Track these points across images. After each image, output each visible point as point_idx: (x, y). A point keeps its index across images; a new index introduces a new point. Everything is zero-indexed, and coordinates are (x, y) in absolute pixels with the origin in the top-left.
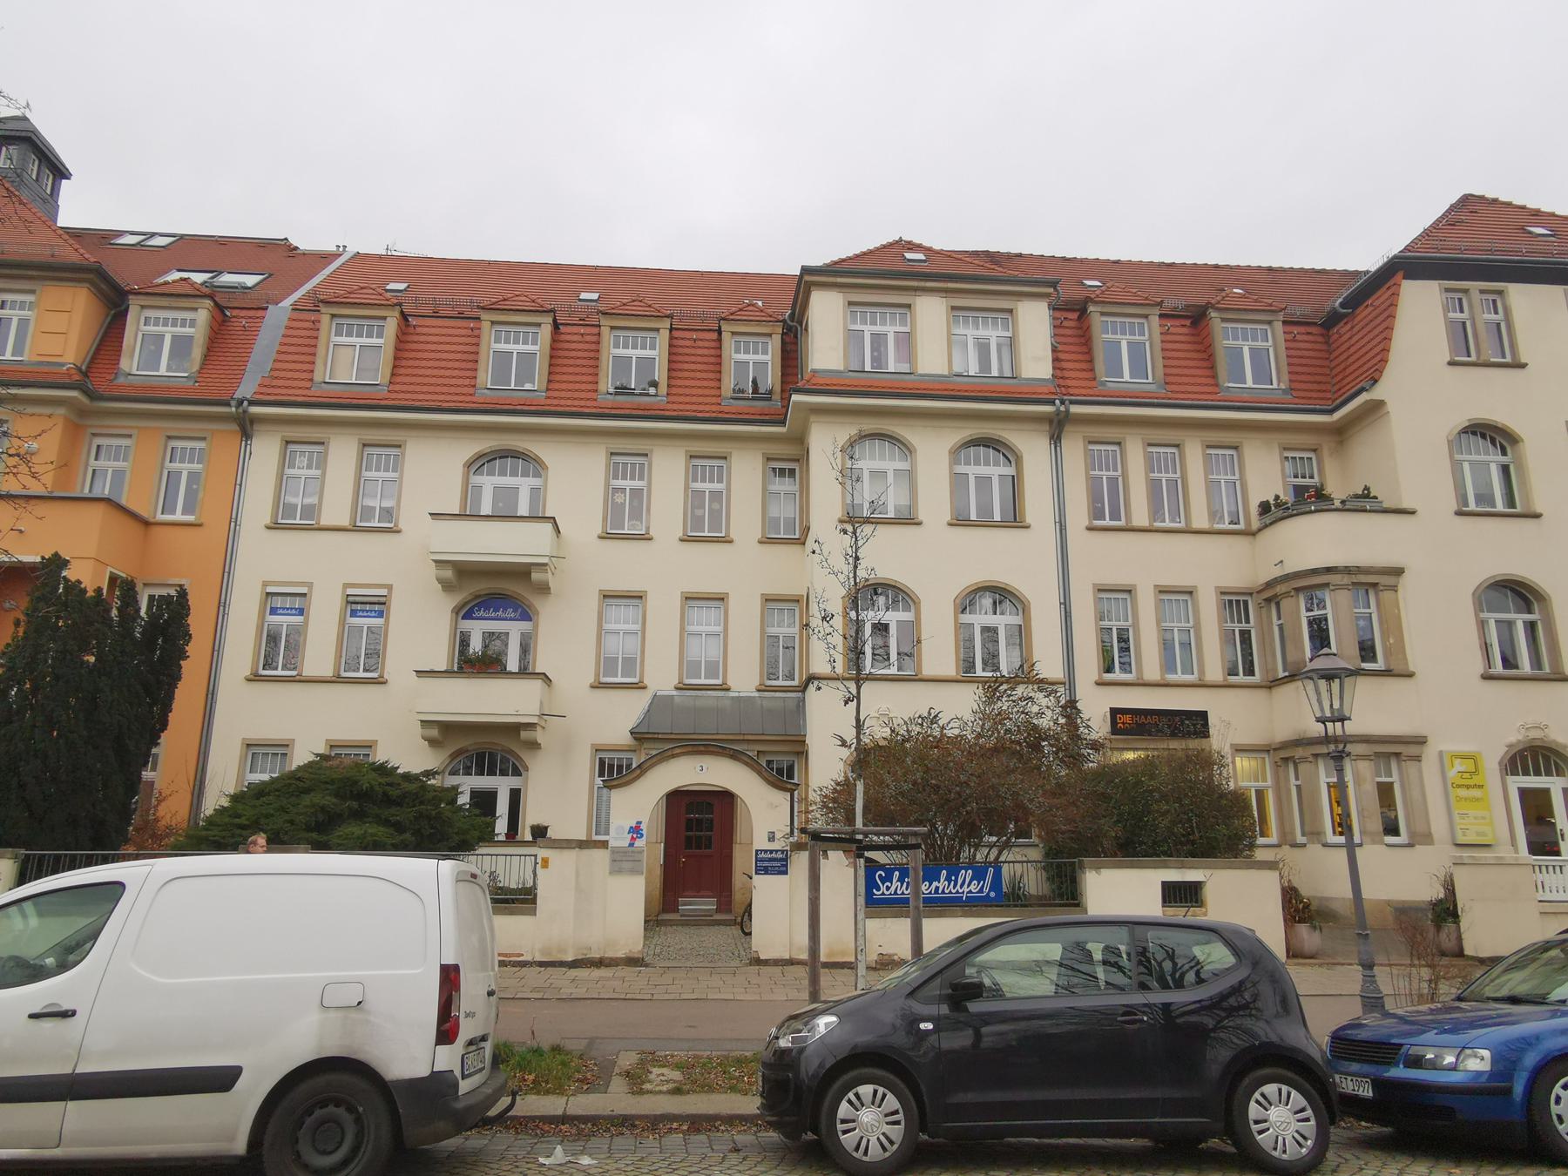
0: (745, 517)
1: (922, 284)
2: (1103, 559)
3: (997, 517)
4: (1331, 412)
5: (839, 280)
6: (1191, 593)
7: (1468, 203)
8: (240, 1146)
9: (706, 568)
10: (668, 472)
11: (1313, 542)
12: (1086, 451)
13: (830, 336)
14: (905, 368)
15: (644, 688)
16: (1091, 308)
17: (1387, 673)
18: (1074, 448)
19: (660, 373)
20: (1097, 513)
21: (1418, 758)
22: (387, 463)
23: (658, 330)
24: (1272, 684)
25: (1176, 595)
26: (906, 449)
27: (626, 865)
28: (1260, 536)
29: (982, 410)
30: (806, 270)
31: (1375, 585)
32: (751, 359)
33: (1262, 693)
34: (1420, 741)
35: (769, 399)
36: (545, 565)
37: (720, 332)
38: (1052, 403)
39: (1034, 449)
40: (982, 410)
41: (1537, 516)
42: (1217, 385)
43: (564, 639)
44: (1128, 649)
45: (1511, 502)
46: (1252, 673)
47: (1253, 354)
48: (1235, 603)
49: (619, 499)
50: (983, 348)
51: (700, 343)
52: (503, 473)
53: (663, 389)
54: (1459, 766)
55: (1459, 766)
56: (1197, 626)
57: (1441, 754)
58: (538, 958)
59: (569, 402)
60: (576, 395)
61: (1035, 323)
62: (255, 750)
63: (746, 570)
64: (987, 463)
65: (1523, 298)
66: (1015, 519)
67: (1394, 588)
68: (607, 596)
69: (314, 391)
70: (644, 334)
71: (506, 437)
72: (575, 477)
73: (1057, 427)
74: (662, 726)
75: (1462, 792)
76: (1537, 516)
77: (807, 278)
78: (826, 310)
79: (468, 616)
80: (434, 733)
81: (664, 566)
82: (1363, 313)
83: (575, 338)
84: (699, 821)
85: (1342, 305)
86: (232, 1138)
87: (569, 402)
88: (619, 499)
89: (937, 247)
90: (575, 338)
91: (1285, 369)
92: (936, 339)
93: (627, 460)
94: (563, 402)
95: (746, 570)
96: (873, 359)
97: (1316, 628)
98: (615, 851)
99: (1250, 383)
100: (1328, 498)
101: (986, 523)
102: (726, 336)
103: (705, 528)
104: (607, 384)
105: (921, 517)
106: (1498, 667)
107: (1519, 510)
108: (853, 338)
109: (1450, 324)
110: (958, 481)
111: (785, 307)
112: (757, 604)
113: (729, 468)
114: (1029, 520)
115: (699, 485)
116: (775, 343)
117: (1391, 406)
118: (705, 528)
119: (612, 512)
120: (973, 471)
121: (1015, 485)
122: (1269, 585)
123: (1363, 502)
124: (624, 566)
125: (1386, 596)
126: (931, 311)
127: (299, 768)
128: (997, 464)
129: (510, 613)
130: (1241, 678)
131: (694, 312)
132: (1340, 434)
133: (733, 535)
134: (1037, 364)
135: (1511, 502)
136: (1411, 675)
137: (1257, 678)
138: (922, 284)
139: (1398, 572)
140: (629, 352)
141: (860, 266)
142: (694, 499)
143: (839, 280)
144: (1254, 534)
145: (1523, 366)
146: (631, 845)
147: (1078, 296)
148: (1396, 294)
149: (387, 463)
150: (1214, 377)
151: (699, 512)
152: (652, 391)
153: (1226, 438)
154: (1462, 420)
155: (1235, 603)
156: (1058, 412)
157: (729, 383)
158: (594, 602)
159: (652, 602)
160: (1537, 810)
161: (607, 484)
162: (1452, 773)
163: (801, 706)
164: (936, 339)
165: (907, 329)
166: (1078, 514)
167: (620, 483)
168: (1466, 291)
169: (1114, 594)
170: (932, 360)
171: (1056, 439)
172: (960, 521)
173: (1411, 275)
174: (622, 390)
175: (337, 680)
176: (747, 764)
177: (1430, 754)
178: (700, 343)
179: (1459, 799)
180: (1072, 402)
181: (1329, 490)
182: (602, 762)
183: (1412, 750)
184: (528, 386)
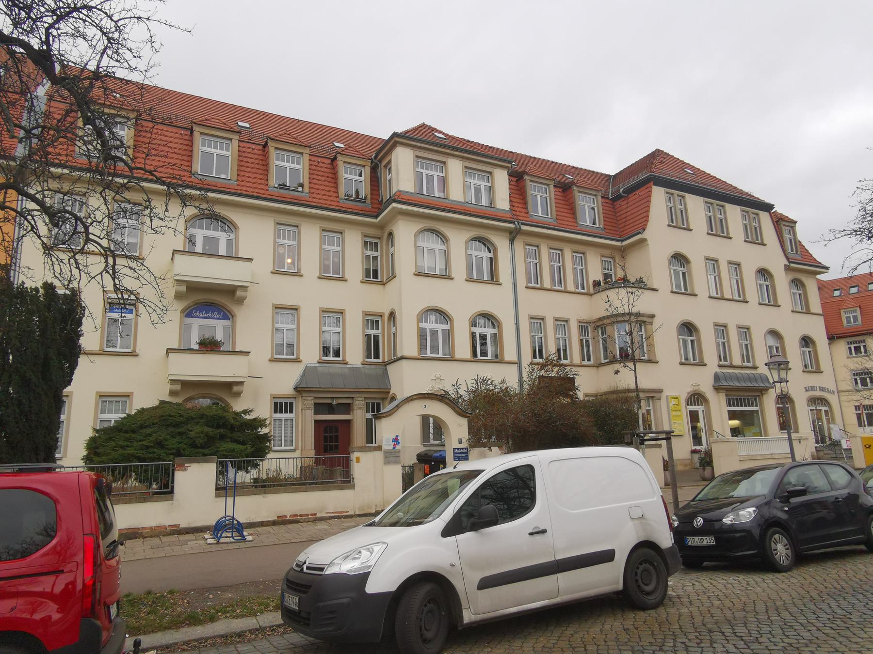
0: (354, 267)
1: (452, 152)
2: (538, 303)
3: (485, 278)
4: (622, 241)
5: (412, 143)
6: (567, 321)
7: (658, 150)
8: (620, 586)
9: (333, 295)
10: (310, 237)
11: (619, 300)
12: (525, 248)
13: (404, 171)
14: (442, 195)
15: (300, 362)
16: (526, 177)
17: (649, 361)
18: (519, 245)
19: (304, 178)
20: (529, 280)
21: (659, 399)
22: (329, 240)
23: (302, 154)
24: (599, 365)
25: (562, 323)
26: (444, 239)
27: (392, 459)
28: (595, 296)
29: (478, 220)
30: (395, 135)
31: (644, 322)
32: (353, 179)
33: (595, 369)
34: (660, 391)
35: (364, 202)
36: (247, 287)
37: (192, 132)
38: (514, 223)
39: (502, 244)
40: (478, 220)
41: (696, 295)
42: (576, 222)
43: (253, 330)
44: (486, 344)
45: (686, 289)
46: (589, 360)
47: (589, 209)
48: (583, 327)
49: (281, 250)
50: (478, 190)
51: (321, 165)
52: (208, 228)
53: (306, 189)
54: (674, 402)
55: (674, 402)
56: (545, 336)
57: (667, 397)
58: (357, 513)
59: (252, 190)
60: (256, 186)
61: (502, 179)
62: (105, 399)
63: (356, 298)
64: (480, 250)
65: (728, 206)
66: (494, 279)
67: (651, 324)
68: (277, 307)
69: (193, 179)
70: (356, 167)
71: (210, 206)
72: (256, 234)
73: (513, 236)
74: (314, 383)
75: (674, 413)
76: (696, 295)
77: (396, 139)
78: (403, 160)
79: (189, 315)
80: (178, 387)
81: (311, 294)
82: (633, 197)
83: (248, 150)
84: (331, 437)
85: (623, 192)
86: (618, 583)
87: (252, 190)
88: (281, 250)
89: (450, 134)
90: (248, 150)
91: (602, 218)
92: (458, 183)
93: (332, 231)
94: (248, 189)
95: (356, 298)
96: (428, 189)
97: (622, 339)
98: (386, 452)
99: (540, 214)
100: (628, 281)
101: (480, 281)
102: (196, 134)
103: (332, 273)
104: (273, 182)
105: (453, 276)
106: (683, 360)
107: (688, 292)
108: (419, 176)
109: (706, 216)
110: (469, 258)
111: (377, 155)
112: (317, 313)
113: (299, 233)
114: (501, 281)
115: (326, 247)
116: (367, 171)
117: (649, 242)
118: (332, 273)
119: (278, 259)
120: (475, 253)
121: (493, 263)
122: (600, 319)
123: (624, 282)
124: (287, 291)
125: (649, 326)
126: (455, 167)
127: (142, 411)
128: (485, 251)
129: (216, 314)
130: (586, 362)
131: (326, 148)
132: (623, 252)
133: (347, 277)
134: (503, 203)
135: (686, 289)
136: (657, 362)
137: (592, 362)
138: (452, 152)
139: (653, 316)
140: (285, 164)
141: (409, 135)
142: (324, 255)
143: (412, 143)
144: (591, 295)
145: (730, 238)
146: (394, 448)
147: (521, 171)
148: (650, 191)
149: (329, 240)
150: (526, 208)
151: (327, 262)
152: (300, 189)
153: (581, 248)
154: (671, 252)
155: (583, 327)
156: (516, 229)
157: (342, 191)
158: (269, 311)
159: (303, 313)
160: (694, 417)
161: (275, 241)
162: (671, 405)
163: (385, 374)
164: (458, 183)
165: (443, 175)
166: (522, 282)
167: (281, 241)
168: (672, 194)
169: (538, 321)
170: (456, 194)
171: (512, 241)
172: (470, 280)
173: (656, 184)
174: (283, 186)
175: (102, 353)
176: (447, 404)
177: (663, 396)
178: (321, 165)
179: (674, 416)
180: (523, 224)
181: (629, 277)
182: (276, 404)
183: (656, 395)
184: (223, 176)
